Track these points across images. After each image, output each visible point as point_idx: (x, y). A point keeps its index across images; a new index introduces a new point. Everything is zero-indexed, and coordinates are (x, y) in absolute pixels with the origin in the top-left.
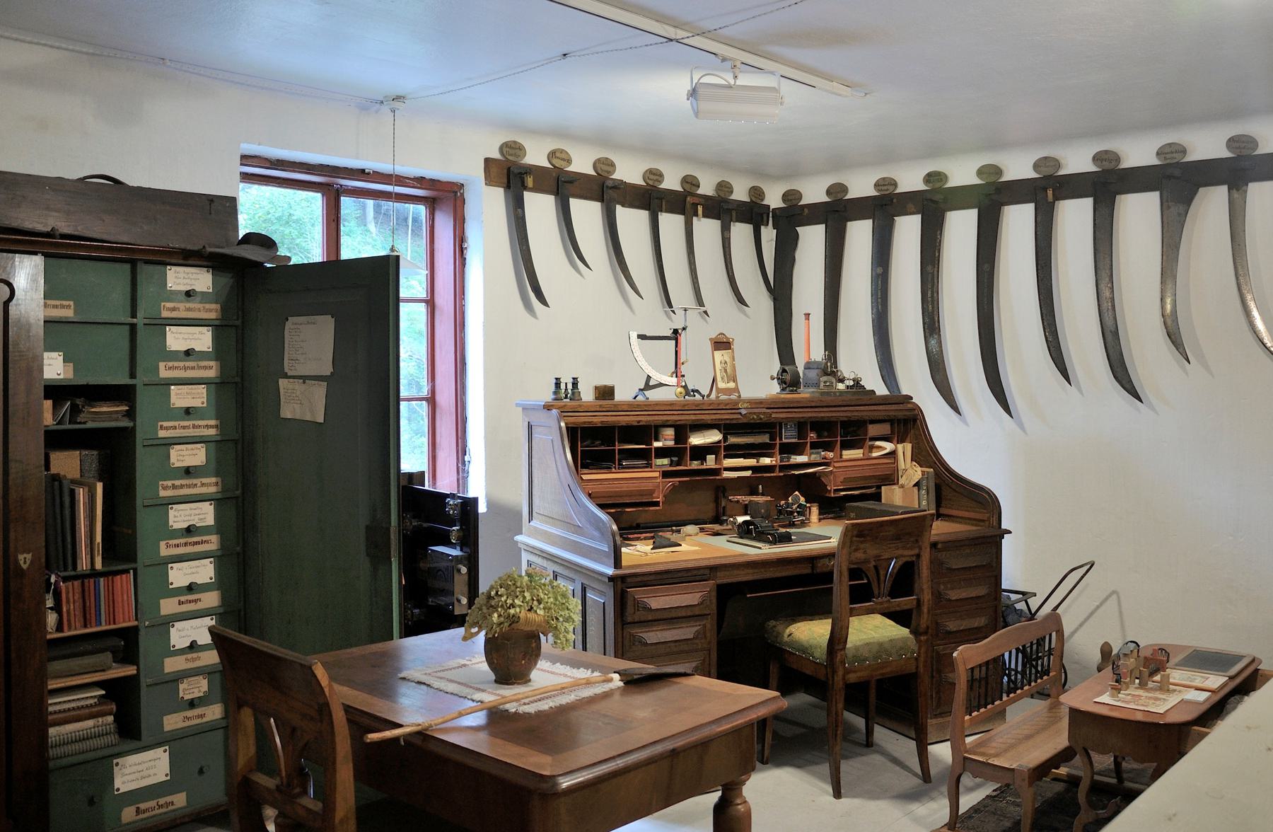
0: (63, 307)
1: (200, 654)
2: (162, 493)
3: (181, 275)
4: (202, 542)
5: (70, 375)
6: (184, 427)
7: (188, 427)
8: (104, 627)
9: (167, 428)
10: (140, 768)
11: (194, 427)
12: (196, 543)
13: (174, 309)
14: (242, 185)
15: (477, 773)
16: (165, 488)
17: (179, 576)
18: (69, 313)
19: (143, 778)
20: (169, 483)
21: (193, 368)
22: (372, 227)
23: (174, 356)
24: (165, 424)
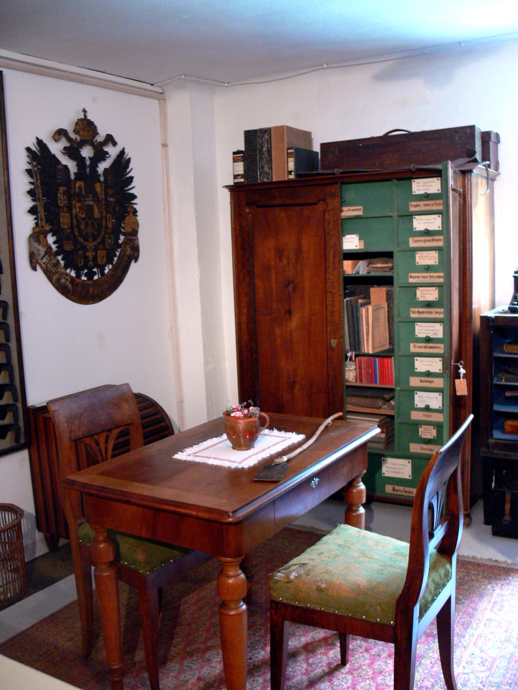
0: (357, 210)
1: (432, 414)
2: (412, 316)
3: (421, 185)
4: (435, 347)
5: (362, 247)
6: (424, 277)
8: (378, 385)
10: (395, 466)
11: (430, 277)
12: (432, 347)
14: (176, 432)
15: (241, 382)
16: (414, 312)
18: (360, 213)
19: (396, 472)
20: (416, 310)
22: (483, 186)
24: (413, 275)
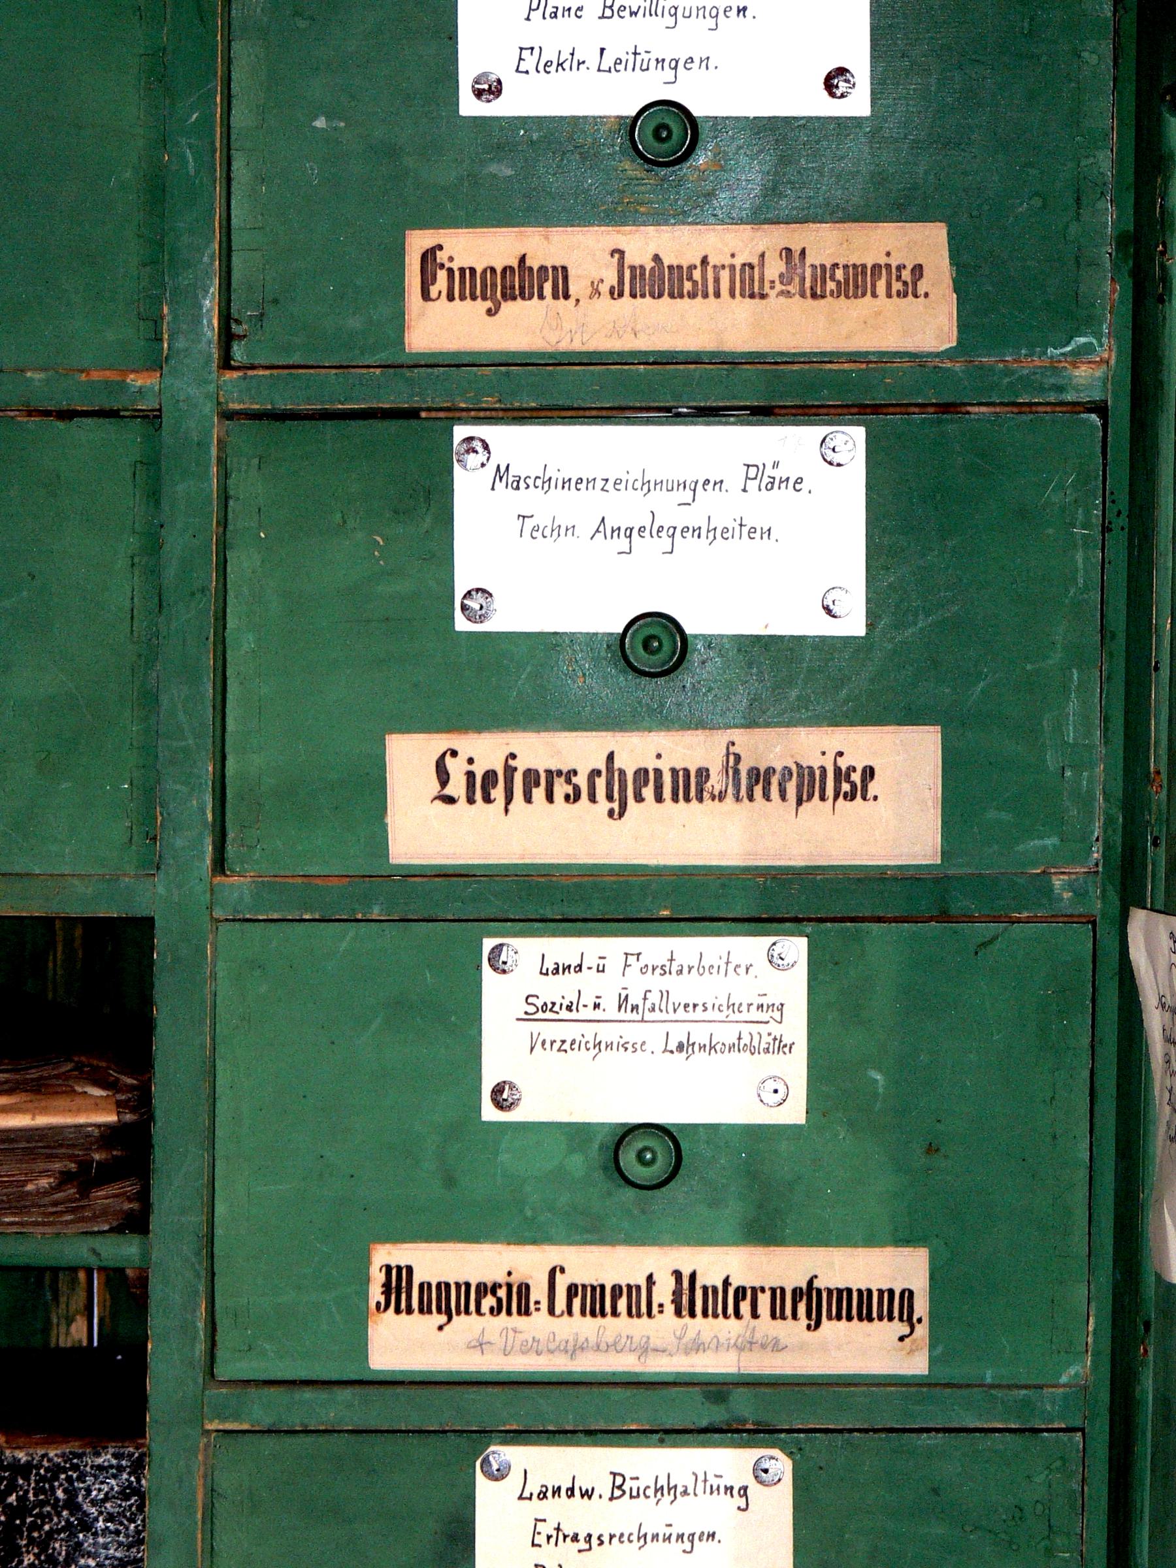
6: (595, 1300)
7: (637, 1300)
9: (447, 1300)
13: (516, 283)
17: (545, 534)
21: (689, 786)
23: (522, 680)
24: (434, 1263)
